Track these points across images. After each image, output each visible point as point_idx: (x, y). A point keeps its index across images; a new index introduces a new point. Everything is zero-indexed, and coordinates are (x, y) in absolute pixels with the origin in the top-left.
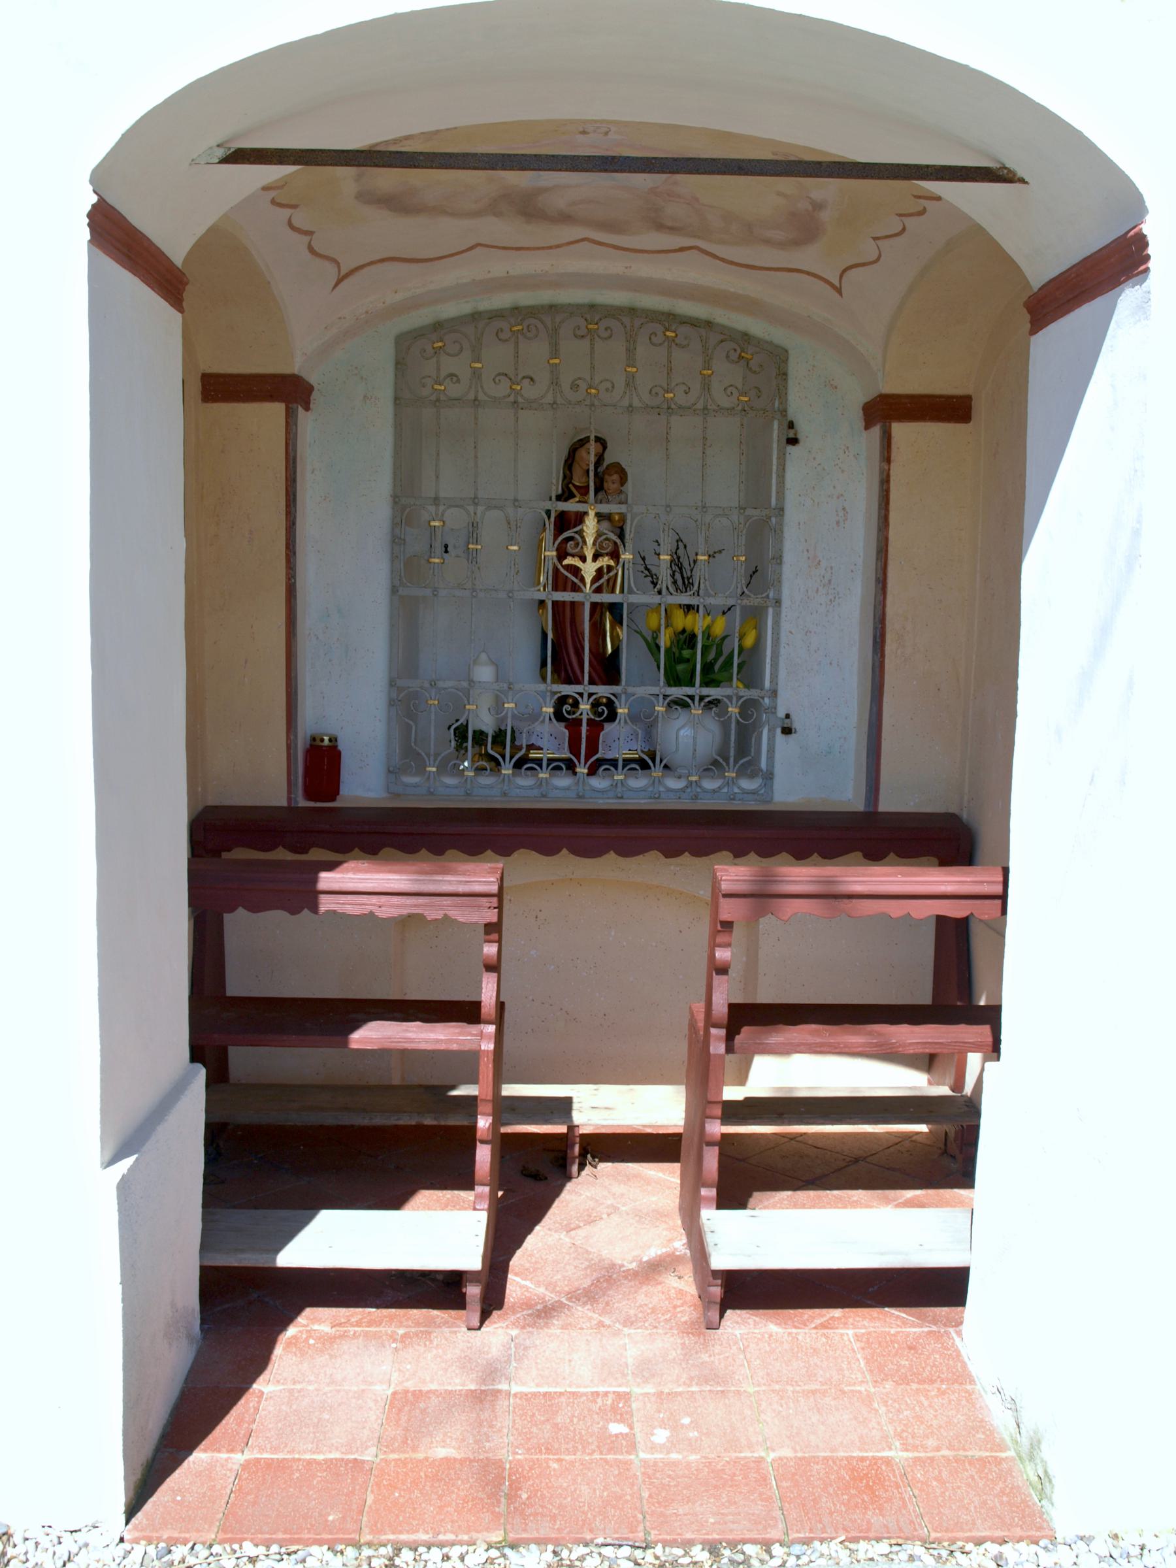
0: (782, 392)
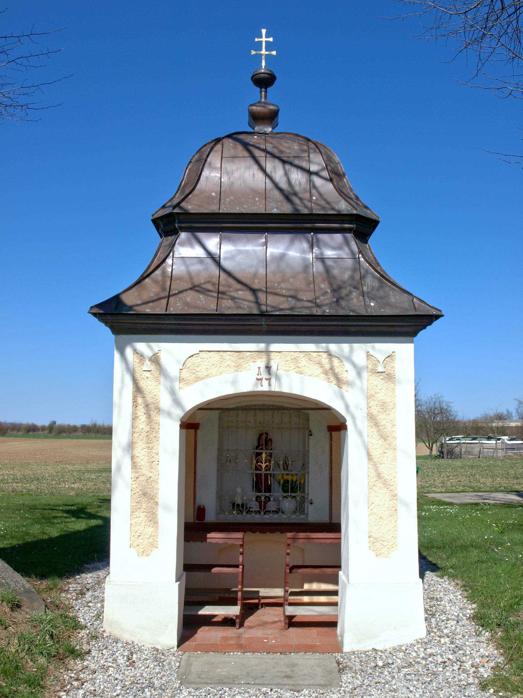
0: (308, 423)
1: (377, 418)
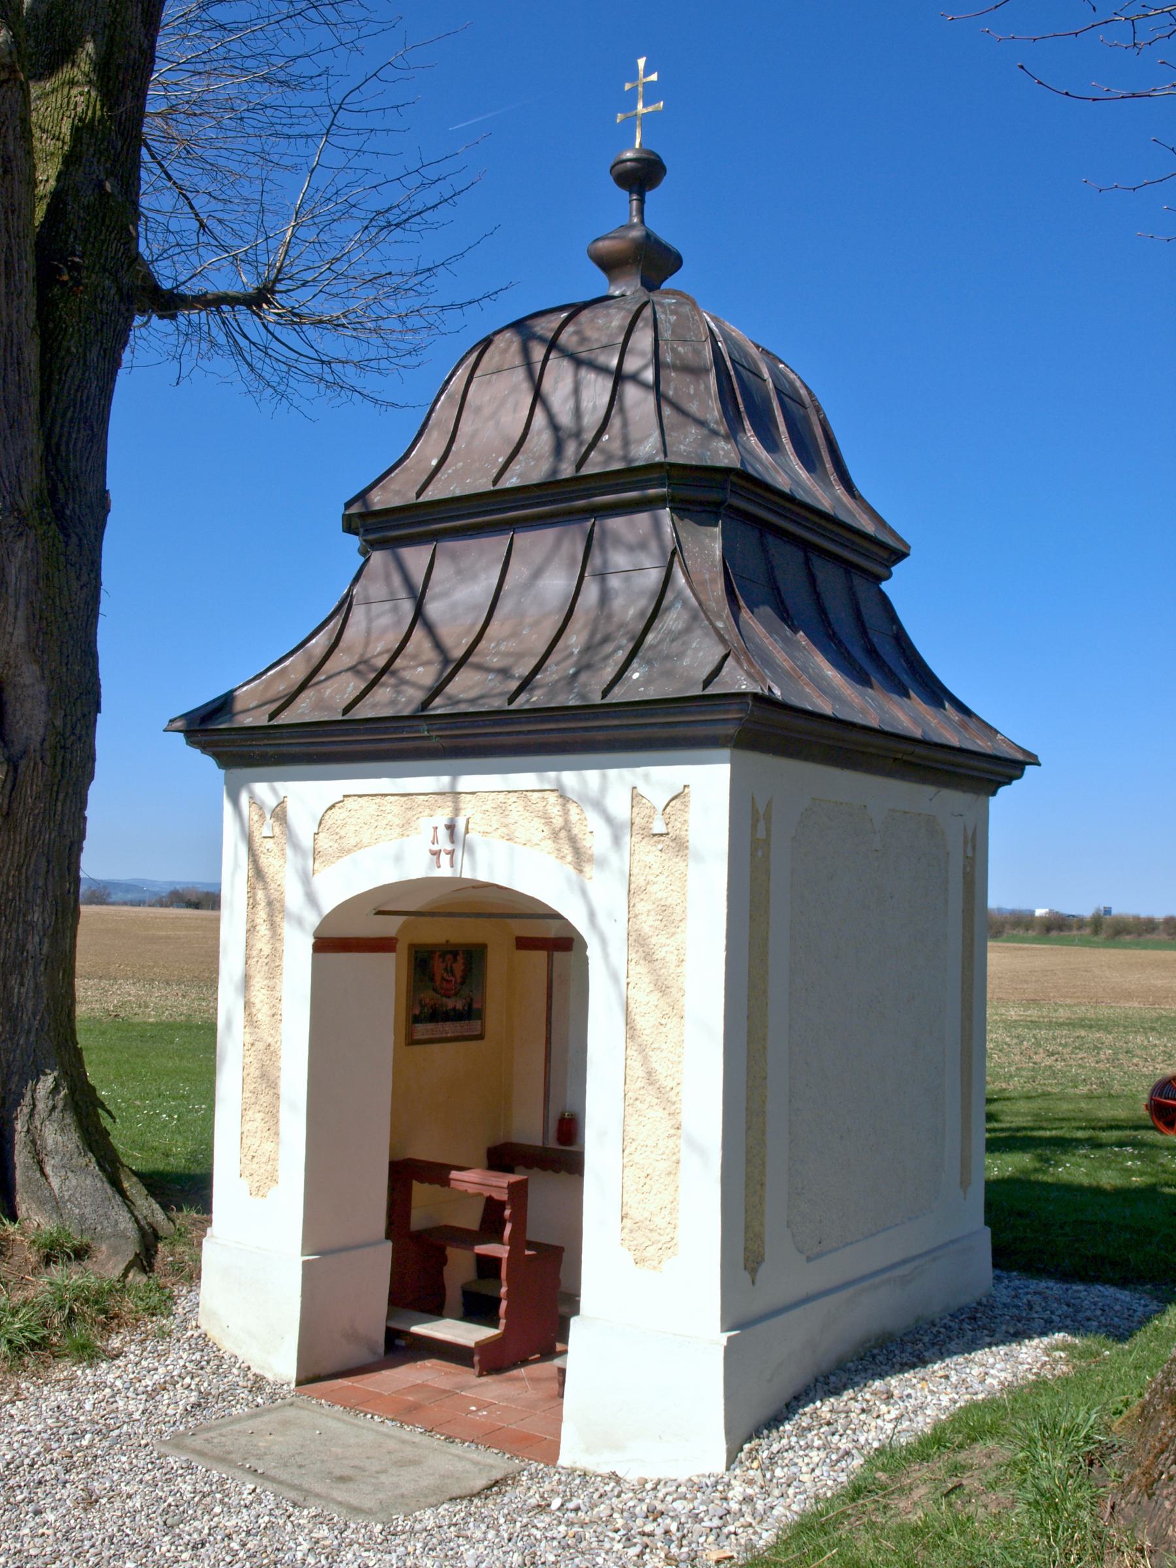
1: (647, 942)
